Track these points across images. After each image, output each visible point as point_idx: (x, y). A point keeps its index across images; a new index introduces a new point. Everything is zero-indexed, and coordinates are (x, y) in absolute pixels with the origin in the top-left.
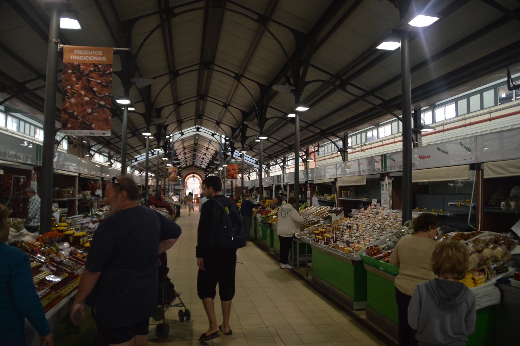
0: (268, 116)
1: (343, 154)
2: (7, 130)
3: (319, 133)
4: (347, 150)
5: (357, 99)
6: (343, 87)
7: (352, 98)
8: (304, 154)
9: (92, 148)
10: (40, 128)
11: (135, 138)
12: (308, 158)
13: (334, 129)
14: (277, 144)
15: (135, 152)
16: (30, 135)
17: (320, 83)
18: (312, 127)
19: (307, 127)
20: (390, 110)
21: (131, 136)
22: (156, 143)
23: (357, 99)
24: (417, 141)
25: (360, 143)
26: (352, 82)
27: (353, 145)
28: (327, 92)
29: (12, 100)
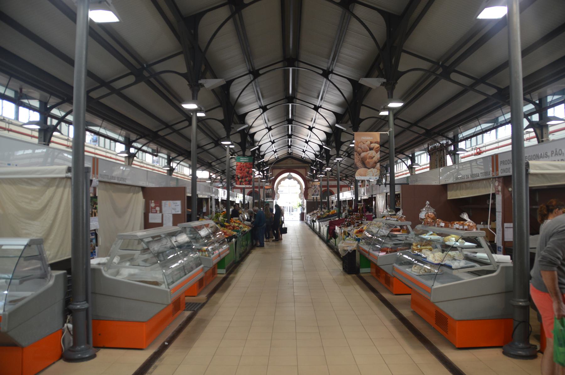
0: (361, 116)
1: (538, 131)
2: (4, 119)
3: (423, 134)
4: (457, 153)
5: (465, 90)
6: (446, 75)
7: (460, 88)
8: (450, 142)
9: (232, 183)
10: (186, 167)
11: (218, 147)
12: (413, 164)
13: (404, 147)
14: (408, 129)
15: (174, 133)
16: (110, 149)
17: (375, 120)
18: (482, 85)
19: (410, 127)
20: (432, 137)
21: (214, 146)
22: (241, 153)
23: (465, 90)
24: (542, 138)
25: (470, 146)
26: (456, 69)
27: (467, 147)
28: (413, 96)
29: (64, 105)
